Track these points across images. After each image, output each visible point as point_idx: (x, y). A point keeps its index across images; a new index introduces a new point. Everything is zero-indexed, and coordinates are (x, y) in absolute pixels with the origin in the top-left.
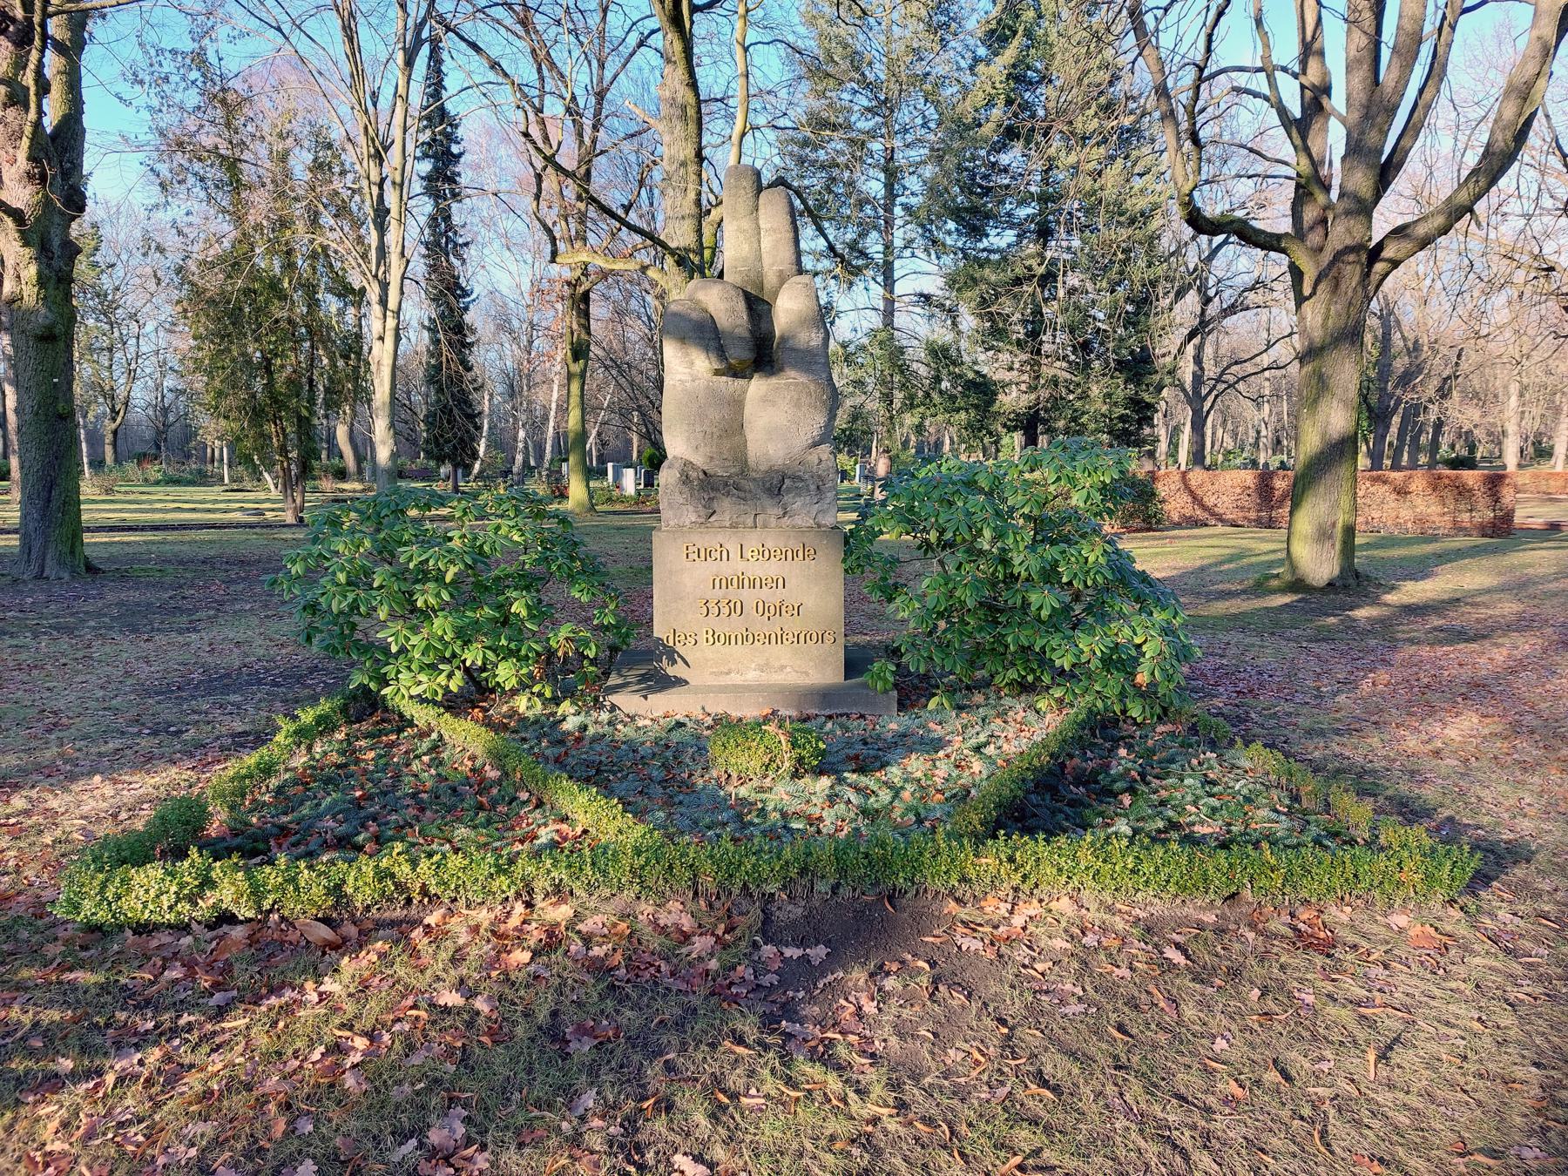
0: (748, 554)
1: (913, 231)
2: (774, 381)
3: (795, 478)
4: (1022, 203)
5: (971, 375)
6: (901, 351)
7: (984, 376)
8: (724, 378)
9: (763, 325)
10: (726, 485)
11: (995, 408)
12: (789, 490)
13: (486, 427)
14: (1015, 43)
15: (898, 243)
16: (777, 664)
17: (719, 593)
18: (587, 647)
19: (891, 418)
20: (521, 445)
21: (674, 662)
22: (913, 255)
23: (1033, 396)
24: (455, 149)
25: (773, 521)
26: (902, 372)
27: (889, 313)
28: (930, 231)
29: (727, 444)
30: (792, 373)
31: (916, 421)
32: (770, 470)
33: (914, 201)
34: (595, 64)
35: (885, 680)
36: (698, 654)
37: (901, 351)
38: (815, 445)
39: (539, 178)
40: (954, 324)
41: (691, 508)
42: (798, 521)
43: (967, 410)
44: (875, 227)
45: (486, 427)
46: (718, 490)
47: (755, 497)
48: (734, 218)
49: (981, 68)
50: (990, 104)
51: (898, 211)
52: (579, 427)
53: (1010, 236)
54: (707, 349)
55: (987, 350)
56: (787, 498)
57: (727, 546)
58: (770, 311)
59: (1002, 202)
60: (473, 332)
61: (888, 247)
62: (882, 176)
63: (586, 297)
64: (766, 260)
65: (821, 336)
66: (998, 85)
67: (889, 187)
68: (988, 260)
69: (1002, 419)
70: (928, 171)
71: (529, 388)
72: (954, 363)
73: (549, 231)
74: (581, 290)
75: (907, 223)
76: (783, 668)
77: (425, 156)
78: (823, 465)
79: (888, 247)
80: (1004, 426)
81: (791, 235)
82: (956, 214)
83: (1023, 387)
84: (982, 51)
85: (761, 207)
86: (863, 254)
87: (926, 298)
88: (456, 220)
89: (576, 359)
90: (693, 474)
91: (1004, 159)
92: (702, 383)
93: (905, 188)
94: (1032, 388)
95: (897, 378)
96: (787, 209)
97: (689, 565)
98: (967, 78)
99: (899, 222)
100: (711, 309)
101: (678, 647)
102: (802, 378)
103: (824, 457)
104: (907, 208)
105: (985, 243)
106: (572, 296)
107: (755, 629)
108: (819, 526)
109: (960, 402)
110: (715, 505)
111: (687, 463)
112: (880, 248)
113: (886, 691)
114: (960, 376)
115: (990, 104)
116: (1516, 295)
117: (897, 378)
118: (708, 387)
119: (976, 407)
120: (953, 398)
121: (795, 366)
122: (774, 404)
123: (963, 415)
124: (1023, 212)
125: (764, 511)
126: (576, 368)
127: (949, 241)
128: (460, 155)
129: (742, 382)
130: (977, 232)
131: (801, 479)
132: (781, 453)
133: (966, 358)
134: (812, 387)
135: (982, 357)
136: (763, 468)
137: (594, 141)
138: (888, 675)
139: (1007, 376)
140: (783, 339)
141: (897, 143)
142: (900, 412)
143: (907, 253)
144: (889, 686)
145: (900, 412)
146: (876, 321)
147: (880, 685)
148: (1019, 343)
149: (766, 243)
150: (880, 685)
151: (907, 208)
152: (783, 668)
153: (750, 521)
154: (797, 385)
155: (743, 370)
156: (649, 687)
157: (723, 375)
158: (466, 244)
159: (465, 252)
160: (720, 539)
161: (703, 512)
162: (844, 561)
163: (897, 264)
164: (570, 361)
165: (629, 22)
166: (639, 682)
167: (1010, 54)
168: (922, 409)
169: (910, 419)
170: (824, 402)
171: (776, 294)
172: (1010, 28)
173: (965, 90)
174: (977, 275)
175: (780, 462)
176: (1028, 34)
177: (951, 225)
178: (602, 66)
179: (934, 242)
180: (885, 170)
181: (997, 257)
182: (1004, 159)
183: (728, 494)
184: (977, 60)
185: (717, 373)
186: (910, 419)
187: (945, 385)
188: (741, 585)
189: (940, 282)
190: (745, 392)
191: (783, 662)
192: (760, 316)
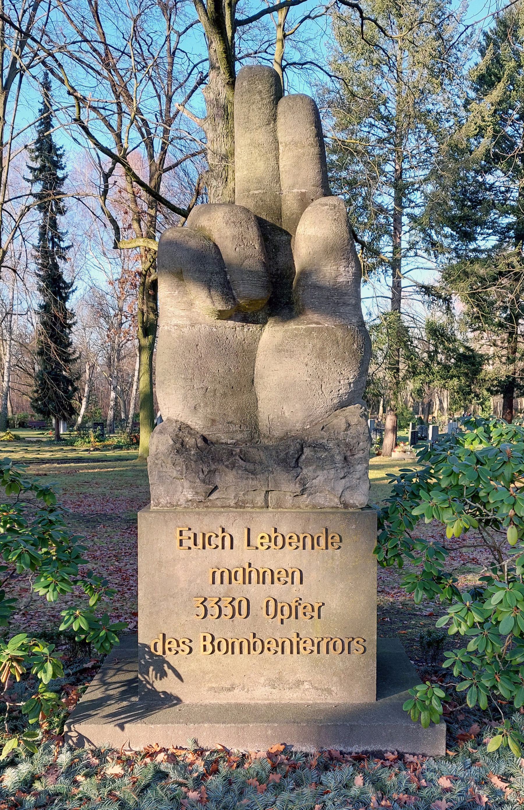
0: (256, 541)
1: (417, 236)
2: (292, 326)
3: (317, 446)
4: (505, 213)
5: (461, 350)
6: (406, 329)
7: (472, 351)
8: (231, 323)
9: (281, 259)
10: (231, 454)
11: (482, 375)
12: (309, 462)
13: (86, 389)
14: (501, 85)
15: (404, 245)
16: (292, 679)
17: (219, 589)
18: (42, 668)
19: (398, 383)
20: (112, 403)
21: (164, 674)
22: (416, 255)
23: (511, 367)
24: (60, 174)
25: (289, 498)
26: (406, 346)
27: (396, 300)
28: (430, 236)
29: (232, 404)
30: (316, 317)
31: (418, 385)
32: (285, 438)
33: (417, 211)
34: (164, 99)
35: (431, 710)
36: (194, 666)
37: (406, 329)
38: (342, 405)
39: (106, 176)
40: (448, 308)
41: (186, 484)
42: (320, 499)
43: (459, 377)
44: (387, 232)
45: (86, 389)
46: (220, 461)
47: (266, 469)
48: (248, 129)
49: (473, 106)
50: (480, 133)
51: (405, 220)
52: (148, 389)
53: (493, 241)
54: (209, 285)
55: (475, 330)
56: (307, 471)
57: (231, 530)
58: (289, 242)
59: (488, 213)
60: (73, 315)
61: (396, 247)
62: (392, 191)
63: (154, 285)
64: (286, 181)
65: (352, 270)
66: (486, 118)
67: (398, 201)
68: (477, 258)
69: (488, 385)
70: (429, 188)
71: (119, 360)
72: (449, 340)
73: (113, 222)
74: (149, 280)
75: (412, 229)
76: (299, 683)
77: (37, 179)
78: (352, 431)
79: (396, 247)
80: (488, 390)
81: (315, 150)
82: (452, 222)
83: (504, 359)
84: (472, 94)
85: (281, 120)
86: (377, 253)
87: (427, 290)
88: (61, 229)
89: (146, 334)
90: (190, 441)
91: (490, 179)
92: (204, 330)
93: (411, 201)
94: (511, 361)
95: (402, 352)
96: (312, 118)
97: (182, 553)
98: (462, 113)
99: (406, 228)
100: (216, 237)
101: (169, 657)
102: (328, 323)
103: (354, 420)
104: (412, 217)
105: (472, 246)
106: (143, 284)
107: (265, 635)
108: (346, 506)
109: (453, 371)
110: (218, 480)
111: (183, 427)
112: (391, 249)
113: (432, 724)
114: (454, 350)
115: (480, 133)
116: (230, 420)
117: (402, 352)
118: (210, 334)
119: (466, 375)
120: (447, 368)
121: (316, 309)
122: (291, 354)
123: (455, 381)
124: (505, 221)
125: (277, 486)
126: (145, 342)
127: (446, 242)
128: (64, 179)
129: (253, 328)
130: (469, 237)
131: (323, 447)
132: (300, 416)
133: (459, 337)
134: (340, 333)
135: (470, 335)
136: (277, 433)
137: (162, 160)
138: (435, 703)
139: (492, 351)
140: (305, 274)
141: (406, 166)
142: (405, 379)
143: (412, 253)
144: (436, 718)
145: (405, 379)
146: (387, 306)
147: (424, 717)
148: (500, 325)
149: (285, 162)
150: (424, 717)
151: (412, 217)
152: (299, 683)
153: (260, 499)
154: (320, 331)
155: (254, 314)
156: (131, 708)
157: (230, 318)
158: (68, 248)
159: (69, 254)
160: (222, 521)
161: (202, 488)
162: (377, 550)
163: (403, 262)
164: (141, 336)
165: (192, 65)
166: (123, 697)
167: (496, 94)
168: (422, 376)
169: (411, 385)
170: (354, 353)
171: (296, 222)
172: (495, 75)
173: (460, 124)
174: (468, 270)
175: (298, 426)
176: (512, 79)
177: (448, 230)
178: (170, 100)
179: (434, 244)
180: (395, 186)
181: (484, 256)
182: (490, 179)
183: (233, 466)
184: (467, 102)
185: (222, 315)
186: (411, 385)
187: (441, 357)
188: (247, 580)
189: (438, 275)
190: (256, 340)
191: (300, 676)
192: (277, 248)
